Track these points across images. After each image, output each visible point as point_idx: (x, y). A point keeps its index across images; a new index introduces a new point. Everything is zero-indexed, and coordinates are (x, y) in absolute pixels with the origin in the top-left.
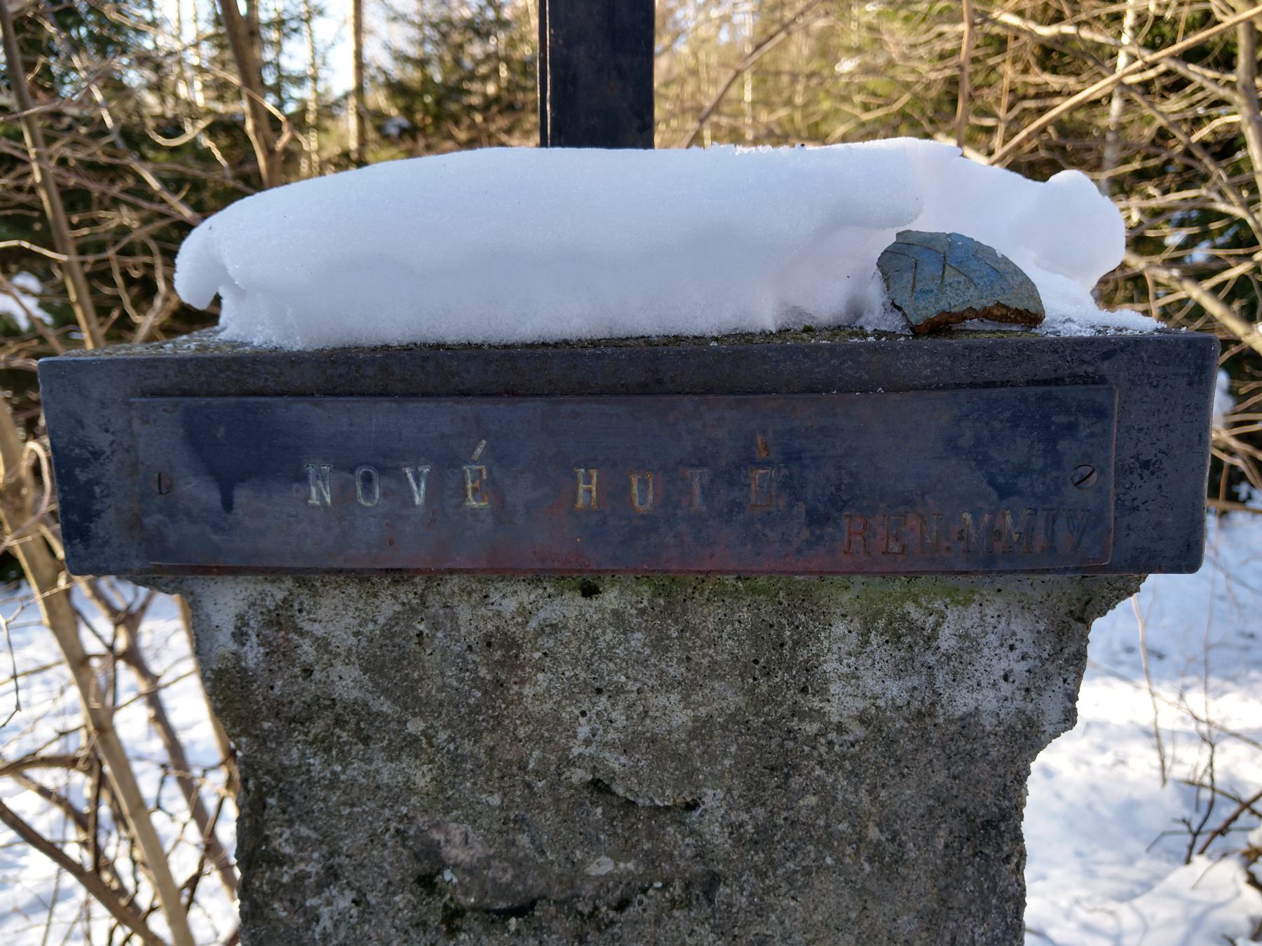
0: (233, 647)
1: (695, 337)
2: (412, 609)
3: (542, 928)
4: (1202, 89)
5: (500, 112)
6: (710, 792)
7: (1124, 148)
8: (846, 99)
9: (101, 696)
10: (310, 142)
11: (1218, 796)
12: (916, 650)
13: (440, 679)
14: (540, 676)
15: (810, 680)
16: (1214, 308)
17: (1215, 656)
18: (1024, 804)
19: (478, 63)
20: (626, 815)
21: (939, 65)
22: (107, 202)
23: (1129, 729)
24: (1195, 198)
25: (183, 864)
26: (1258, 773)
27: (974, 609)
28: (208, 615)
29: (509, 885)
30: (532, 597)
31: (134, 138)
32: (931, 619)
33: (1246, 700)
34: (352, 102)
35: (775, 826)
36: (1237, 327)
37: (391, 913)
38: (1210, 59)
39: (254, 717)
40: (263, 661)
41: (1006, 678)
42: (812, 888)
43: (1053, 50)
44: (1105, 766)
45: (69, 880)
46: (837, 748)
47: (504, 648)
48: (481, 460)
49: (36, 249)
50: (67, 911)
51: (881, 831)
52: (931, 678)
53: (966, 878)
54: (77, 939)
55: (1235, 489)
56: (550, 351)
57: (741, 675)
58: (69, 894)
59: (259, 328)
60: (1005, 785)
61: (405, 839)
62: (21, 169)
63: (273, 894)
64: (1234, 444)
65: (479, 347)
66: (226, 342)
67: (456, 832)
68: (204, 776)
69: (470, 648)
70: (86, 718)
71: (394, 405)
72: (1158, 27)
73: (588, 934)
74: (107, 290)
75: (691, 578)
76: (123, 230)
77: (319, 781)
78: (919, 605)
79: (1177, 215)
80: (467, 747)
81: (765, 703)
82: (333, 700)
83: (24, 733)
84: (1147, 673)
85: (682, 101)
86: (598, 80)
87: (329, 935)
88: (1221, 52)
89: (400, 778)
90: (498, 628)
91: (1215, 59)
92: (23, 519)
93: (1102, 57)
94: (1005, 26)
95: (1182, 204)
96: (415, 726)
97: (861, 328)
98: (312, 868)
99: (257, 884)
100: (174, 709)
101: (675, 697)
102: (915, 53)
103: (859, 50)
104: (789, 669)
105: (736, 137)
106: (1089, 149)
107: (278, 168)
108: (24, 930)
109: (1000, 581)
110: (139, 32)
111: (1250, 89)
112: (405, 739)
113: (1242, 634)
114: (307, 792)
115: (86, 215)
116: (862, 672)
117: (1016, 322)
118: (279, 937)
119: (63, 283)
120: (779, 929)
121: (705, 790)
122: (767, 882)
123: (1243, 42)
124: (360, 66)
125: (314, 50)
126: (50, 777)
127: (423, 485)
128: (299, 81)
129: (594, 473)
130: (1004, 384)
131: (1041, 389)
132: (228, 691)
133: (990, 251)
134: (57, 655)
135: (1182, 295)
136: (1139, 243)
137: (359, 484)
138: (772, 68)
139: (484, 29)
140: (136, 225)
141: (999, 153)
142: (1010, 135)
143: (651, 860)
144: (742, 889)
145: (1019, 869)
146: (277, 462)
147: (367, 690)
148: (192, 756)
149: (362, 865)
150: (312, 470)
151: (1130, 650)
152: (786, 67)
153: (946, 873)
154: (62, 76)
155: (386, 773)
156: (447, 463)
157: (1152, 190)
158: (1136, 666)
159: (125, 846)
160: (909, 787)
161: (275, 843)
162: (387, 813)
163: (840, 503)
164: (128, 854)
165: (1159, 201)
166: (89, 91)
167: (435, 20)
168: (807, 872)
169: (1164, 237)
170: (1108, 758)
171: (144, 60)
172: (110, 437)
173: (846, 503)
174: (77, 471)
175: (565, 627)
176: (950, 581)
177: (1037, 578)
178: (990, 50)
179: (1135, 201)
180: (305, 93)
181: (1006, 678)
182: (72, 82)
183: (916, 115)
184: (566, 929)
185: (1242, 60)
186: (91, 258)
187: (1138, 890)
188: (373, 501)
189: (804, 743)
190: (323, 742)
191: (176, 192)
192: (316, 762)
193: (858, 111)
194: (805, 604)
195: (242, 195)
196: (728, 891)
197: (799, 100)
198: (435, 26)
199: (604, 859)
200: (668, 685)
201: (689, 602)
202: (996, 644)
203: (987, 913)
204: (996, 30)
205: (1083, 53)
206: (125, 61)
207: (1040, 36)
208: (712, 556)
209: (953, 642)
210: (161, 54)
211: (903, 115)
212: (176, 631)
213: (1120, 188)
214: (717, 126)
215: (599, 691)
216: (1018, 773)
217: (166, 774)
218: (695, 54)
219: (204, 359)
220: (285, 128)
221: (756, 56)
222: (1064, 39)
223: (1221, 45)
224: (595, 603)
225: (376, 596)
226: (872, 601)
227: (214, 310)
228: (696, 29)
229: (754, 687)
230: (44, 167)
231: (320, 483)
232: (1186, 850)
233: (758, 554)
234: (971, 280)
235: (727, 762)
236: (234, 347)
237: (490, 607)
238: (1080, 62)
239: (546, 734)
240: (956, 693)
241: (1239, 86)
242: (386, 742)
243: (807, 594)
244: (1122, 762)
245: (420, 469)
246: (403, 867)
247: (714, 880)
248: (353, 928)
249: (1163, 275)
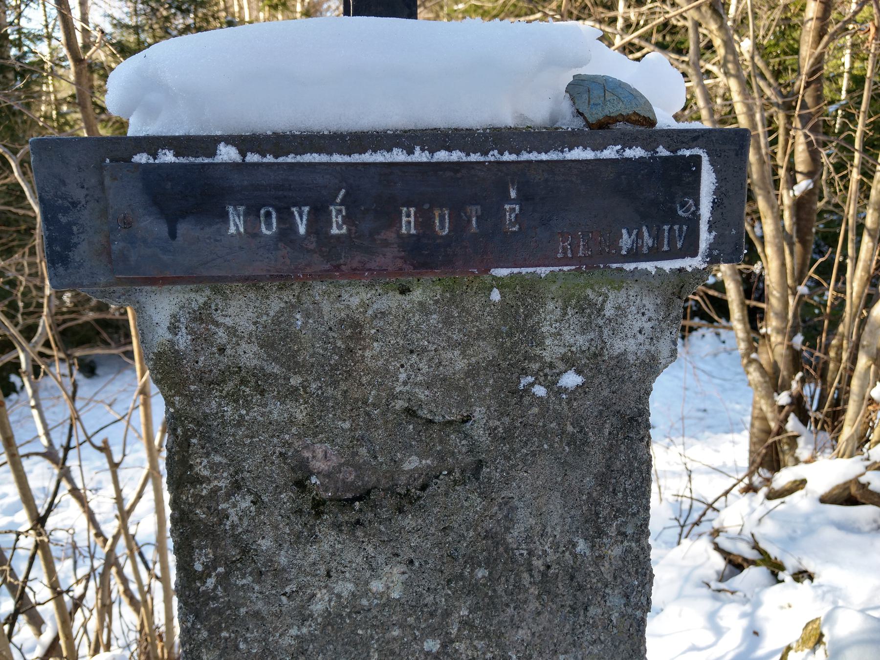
0: (169, 336)
2: (292, 306)
6: (478, 409)
14: (375, 344)
15: (535, 337)
29: (352, 483)
30: (369, 295)
32: (601, 299)
39: (185, 382)
41: (640, 332)
47: (354, 328)
48: (341, 204)
52: (601, 332)
53: (621, 452)
57: (495, 337)
69: (331, 329)
80: (330, 391)
82: (240, 367)
90: (348, 315)
99: (184, 498)
101: (457, 353)
104: (522, 332)
112: (288, 390)
116: (563, 331)
127: (305, 218)
128: (37, 38)
144: (496, 468)
145: (648, 445)
153: (610, 450)
162: (275, 440)
174: (60, 216)
175: (390, 313)
181: (640, 332)
196: (488, 470)
199: (414, 458)
200: (453, 345)
202: (635, 312)
203: (632, 472)
209: (612, 312)
215: (412, 352)
224: (408, 298)
226: (568, 288)
229: (503, 343)
232: (677, 537)
235: (488, 390)
241: (691, 63)
247: (480, 464)
248: (253, 519)
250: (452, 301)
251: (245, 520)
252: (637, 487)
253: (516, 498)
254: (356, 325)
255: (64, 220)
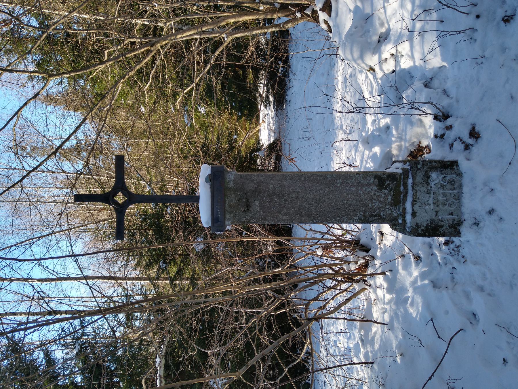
47: (229, 206)
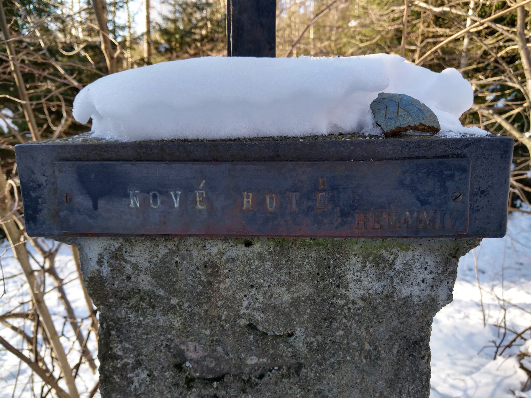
0: (97, 267)
1: (293, 137)
2: (173, 251)
3: (227, 386)
4: (502, 34)
5: (208, 42)
6: (299, 329)
7: (470, 59)
8: (353, 37)
9: (39, 287)
10: (127, 54)
11: (507, 331)
12: (386, 269)
13: (185, 281)
14: (227, 280)
15: (341, 282)
16: (507, 126)
17: (506, 272)
18: (430, 334)
19: (198, 21)
20: (263, 339)
21: (392, 24)
22: (41, 79)
23: (474, 304)
24: (499, 80)
25: (73, 359)
26: (522, 321)
27: (410, 252)
28: (86, 254)
29: (213, 368)
31: (53, 52)
32: (392, 257)
33: (519, 291)
34: (145, 37)
35: (326, 343)
36: (516, 134)
37: (164, 380)
38: (505, 22)
39: (106, 297)
40: (110, 273)
41: (423, 281)
42: (341, 369)
43: (440, 18)
44: (460, 319)
45: (25, 365)
46: (352, 310)
47: (212, 268)
49: (12, 98)
50: (23, 379)
51: (370, 346)
53: (406, 365)
54: (28, 391)
55: (515, 202)
56: (232, 143)
57: (312, 280)
58: (24, 372)
59: (109, 132)
60: (423, 327)
61: (170, 349)
62: (5, 65)
63: (114, 372)
64: (515, 183)
65: (202, 141)
66: (94, 138)
67: (191, 345)
68: (82, 322)
69: (197, 268)
70: (32, 297)
71: (166, 165)
72: (484, 9)
73: (247, 389)
74: (41, 116)
75: (291, 239)
76: (49, 91)
77: (133, 324)
78: (387, 251)
79: (492, 87)
80: (196, 310)
81: (322, 292)
82: (140, 290)
83: (5, 303)
84: (478, 279)
85: (284, 38)
86: (252, 28)
87: (138, 389)
88: (510, 19)
89: (168, 323)
90: (209, 260)
91: (508, 22)
92: (6, 213)
93: (461, 20)
94: (420, 7)
95: (493, 82)
96: (174, 301)
97: (363, 134)
98: (130, 361)
99: (107, 368)
100: (69, 294)
101: (284, 289)
102: (382, 18)
103: (359, 17)
105: (307, 53)
106: (455, 59)
107: (115, 65)
108: (5, 387)
109: (421, 241)
110: (55, 7)
111: (522, 35)
112: (170, 306)
113: (517, 263)
114: (128, 329)
115: (33, 84)
116: (363, 279)
117: (428, 131)
118: (116, 390)
119: (23, 113)
120: (327, 387)
121: (296, 328)
122: (322, 367)
123: (519, 14)
124: (149, 22)
125: (129, 16)
126: (17, 322)
127: (178, 199)
128: (123, 28)
129: (251, 194)
130: (423, 158)
131: (439, 160)
132: (94, 287)
133: (417, 102)
134: (20, 270)
135: (493, 121)
136: (478, 100)
137: (151, 199)
138: (322, 24)
139: (201, 7)
140: (54, 88)
141: (417, 62)
142: (422, 54)
143: (273, 358)
144: (312, 370)
145: (428, 361)
146: (117, 189)
147: (154, 286)
148: (77, 313)
149: (151, 360)
150: (131, 193)
151: (471, 270)
152: (328, 24)
153: (398, 364)
154: (22, 25)
155: (162, 321)
156: (188, 190)
157: (481, 77)
158: (473, 277)
159: (49, 351)
160: (382, 327)
161: (115, 350)
162: (162, 338)
163: (354, 208)
164: (50, 355)
165: (484, 81)
166: (34, 31)
167: (180, 3)
168: (339, 363)
169: (486, 96)
170: (462, 315)
171: (57, 19)
172: (46, 178)
173: (357, 207)
174: (31, 192)
175: (238, 259)
176: (400, 240)
177: (437, 239)
178: (414, 17)
179: (474, 81)
180: (126, 33)
181: (423, 281)
182: (27, 28)
183: (383, 45)
184: (237, 387)
185: (519, 22)
186: (35, 103)
187: (474, 371)
188: (157, 206)
189: (338, 309)
190: (135, 307)
191: (71, 74)
192: (132, 316)
193: (358, 43)
194: (339, 250)
195: (101, 76)
196: (306, 371)
197: (333, 38)
198: (180, 5)
199: (253, 357)
200: (281, 284)
201: (290, 249)
202: (419, 267)
203: (414, 380)
204: (416, 9)
205: (453, 19)
206: (49, 19)
207: (435, 12)
208: (300, 230)
209: (401, 266)
210: (65, 16)
211: (377, 45)
212: (70, 260)
213: (468, 75)
214: (299, 48)
215: (252, 286)
216: (428, 321)
217: (66, 321)
218: (290, 18)
219: (85, 145)
220: (118, 48)
221: (316, 19)
222: (445, 13)
223: (510, 16)
224: (250, 249)
225: (158, 246)
226: (367, 249)
227: (89, 125)
228: (290, 7)
229: (317, 285)
230: (16, 63)
231: (135, 198)
232: (494, 354)
233: (320, 229)
234: (410, 114)
235: (306, 317)
236: (98, 140)
237: (206, 251)
238: (451, 23)
239: (230, 305)
240: (402, 288)
241: (518, 33)
242: (162, 308)
243: (340, 246)
244: (467, 317)
245: (177, 192)
246: (169, 361)
247: (300, 366)
248: (148, 386)
249: (485, 112)
250: (281, 253)
251: (143, 386)
252: (418, 391)
253: (326, 391)
254: (215, 266)
255: (33, 195)
